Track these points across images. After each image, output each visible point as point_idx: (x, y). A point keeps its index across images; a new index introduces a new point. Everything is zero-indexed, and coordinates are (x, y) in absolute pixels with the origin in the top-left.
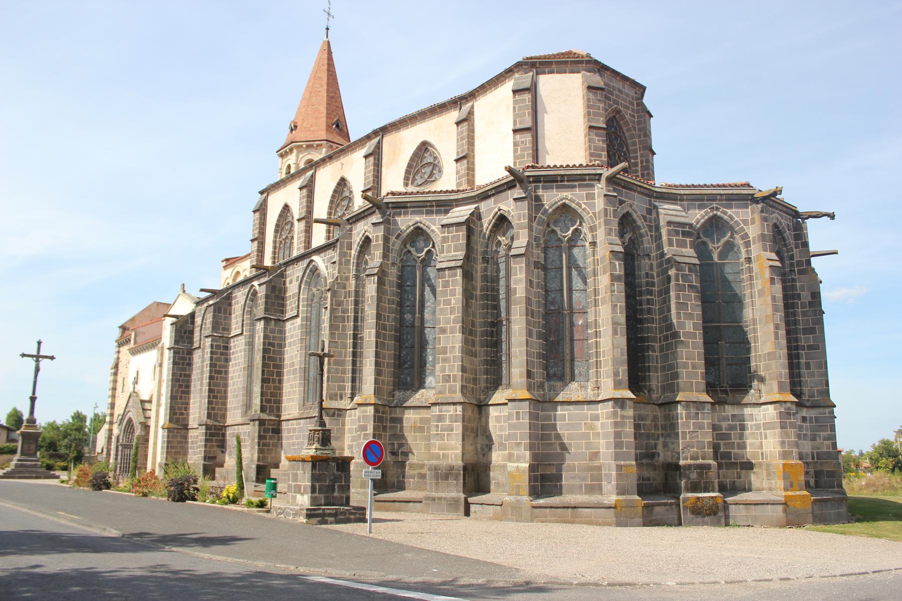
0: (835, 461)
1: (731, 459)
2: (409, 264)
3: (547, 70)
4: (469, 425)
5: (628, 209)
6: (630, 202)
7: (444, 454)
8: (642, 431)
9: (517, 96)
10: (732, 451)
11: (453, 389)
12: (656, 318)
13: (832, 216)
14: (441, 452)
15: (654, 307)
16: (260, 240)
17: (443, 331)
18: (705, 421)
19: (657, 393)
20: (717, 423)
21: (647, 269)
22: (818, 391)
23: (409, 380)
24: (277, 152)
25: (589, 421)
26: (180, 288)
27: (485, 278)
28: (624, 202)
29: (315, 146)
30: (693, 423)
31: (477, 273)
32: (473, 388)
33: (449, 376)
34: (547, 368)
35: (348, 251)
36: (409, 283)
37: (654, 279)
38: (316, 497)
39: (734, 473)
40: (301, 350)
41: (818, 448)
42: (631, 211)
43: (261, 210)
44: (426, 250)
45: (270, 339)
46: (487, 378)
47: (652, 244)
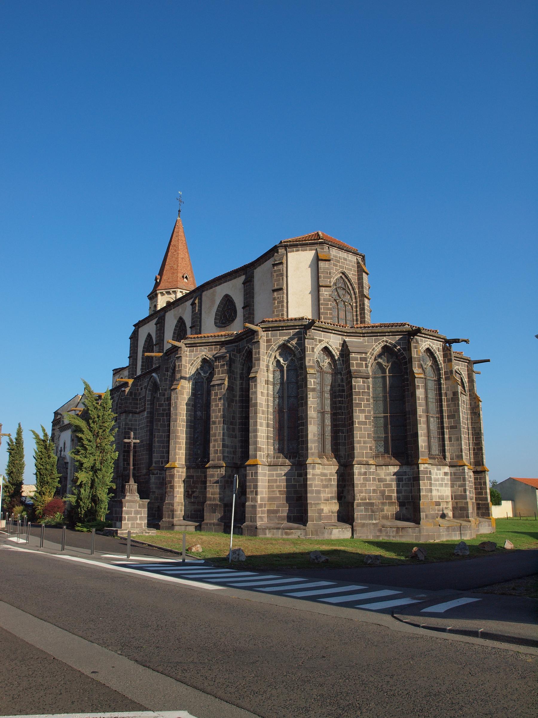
0: (465, 501)
1: (392, 500)
2: (199, 381)
3: (295, 249)
4: (229, 480)
5: (326, 345)
6: (327, 340)
7: (214, 498)
8: (333, 483)
9: (275, 267)
10: (393, 495)
11: (220, 458)
12: (345, 412)
13: (466, 341)
14: (212, 496)
15: (344, 405)
16: (133, 356)
17: (214, 423)
18: (371, 477)
19: (345, 459)
20: (383, 477)
21: (339, 381)
22: (456, 455)
23: (199, 452)
24: (148, 296)
25: (296, 477)
26: (309, 263)
27: (242, 389)
28: (323, 340)
29: (171, 292)
30: (363, 477)
31: (236, 386)
32: (233, 457)
33: (217, 450)
34: (274, 445)
35: (166, 373)
36: (199, 393)
37: (344, 387)
38: (126, 523)
39: (393, 508)
40: (147, 432)
41: (455, 492)
42: (328, 346)
43: (134, 337)
44: (209, 372)
45: (129, 426)
46: (242, 451)
47: (343, 365)
